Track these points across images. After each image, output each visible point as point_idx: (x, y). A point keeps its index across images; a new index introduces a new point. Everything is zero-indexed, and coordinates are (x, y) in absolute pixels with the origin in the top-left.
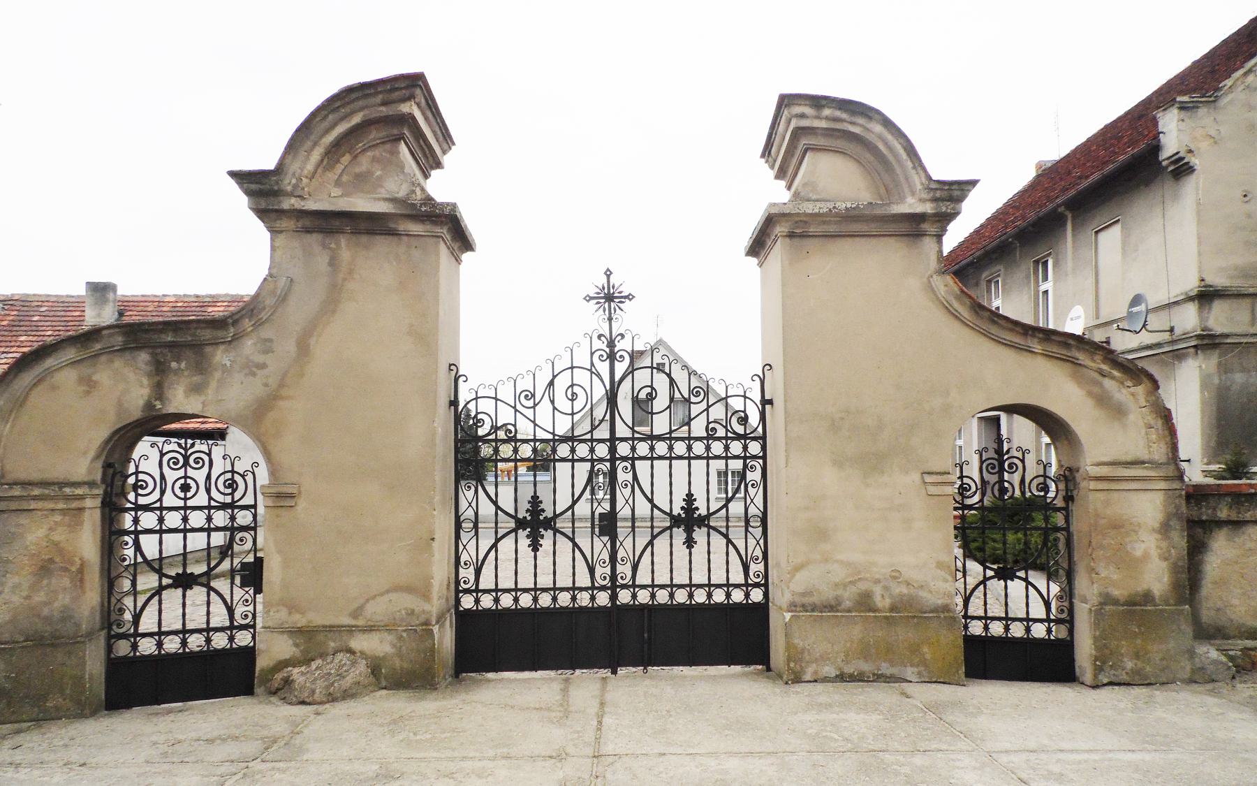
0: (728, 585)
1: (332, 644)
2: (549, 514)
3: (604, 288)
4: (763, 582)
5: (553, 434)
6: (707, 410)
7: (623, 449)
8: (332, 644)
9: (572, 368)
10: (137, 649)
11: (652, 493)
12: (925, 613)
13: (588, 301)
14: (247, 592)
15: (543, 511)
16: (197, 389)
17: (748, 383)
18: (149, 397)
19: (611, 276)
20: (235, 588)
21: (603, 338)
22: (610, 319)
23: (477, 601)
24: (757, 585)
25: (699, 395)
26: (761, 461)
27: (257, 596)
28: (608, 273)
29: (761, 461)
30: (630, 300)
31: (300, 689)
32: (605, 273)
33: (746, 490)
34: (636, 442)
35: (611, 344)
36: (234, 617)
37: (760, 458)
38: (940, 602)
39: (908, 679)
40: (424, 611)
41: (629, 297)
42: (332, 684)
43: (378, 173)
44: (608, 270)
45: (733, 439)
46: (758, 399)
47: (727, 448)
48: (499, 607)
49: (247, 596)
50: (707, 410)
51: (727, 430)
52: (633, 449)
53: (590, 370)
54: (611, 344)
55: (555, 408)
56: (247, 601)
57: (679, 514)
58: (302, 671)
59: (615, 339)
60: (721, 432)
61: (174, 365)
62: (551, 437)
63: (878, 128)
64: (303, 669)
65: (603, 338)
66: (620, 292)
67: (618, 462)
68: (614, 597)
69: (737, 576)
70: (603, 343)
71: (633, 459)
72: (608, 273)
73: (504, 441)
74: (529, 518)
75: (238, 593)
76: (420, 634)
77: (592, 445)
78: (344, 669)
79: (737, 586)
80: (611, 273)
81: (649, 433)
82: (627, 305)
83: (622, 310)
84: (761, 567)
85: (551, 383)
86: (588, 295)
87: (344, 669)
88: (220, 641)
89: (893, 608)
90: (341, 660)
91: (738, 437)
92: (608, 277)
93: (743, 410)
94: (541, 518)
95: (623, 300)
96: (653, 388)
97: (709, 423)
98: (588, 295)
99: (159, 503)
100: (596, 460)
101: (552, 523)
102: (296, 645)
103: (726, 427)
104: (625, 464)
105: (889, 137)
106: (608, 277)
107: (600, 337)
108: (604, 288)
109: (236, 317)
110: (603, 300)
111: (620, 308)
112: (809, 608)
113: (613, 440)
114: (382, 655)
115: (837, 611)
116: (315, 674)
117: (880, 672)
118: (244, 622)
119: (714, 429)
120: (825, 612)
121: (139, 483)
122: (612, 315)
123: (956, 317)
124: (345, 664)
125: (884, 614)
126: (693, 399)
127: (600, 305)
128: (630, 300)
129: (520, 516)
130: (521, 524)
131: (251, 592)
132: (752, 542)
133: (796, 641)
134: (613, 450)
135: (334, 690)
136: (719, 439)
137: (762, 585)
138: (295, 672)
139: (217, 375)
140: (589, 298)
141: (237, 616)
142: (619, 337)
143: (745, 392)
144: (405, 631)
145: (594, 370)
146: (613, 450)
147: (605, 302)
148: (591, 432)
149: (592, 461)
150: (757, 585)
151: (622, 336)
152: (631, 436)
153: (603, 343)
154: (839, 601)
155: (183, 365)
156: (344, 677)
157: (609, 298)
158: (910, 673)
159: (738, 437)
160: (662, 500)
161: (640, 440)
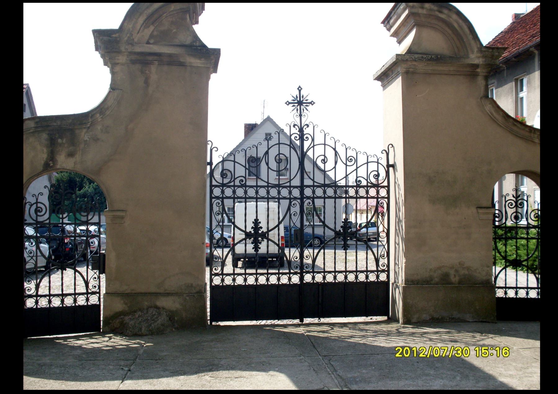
0: (367, 271)
1: (146, 303)
2: (264, 230)
3: (297, 97)
4: (386, 269)
5: (268, 183)
6: (356, 170)
7: (308, 192)
8: (146, 303)
9: (279, 144)
10: (38, 304)
11: (324, 217)
12: (476, 284)
13: (288, 105)
14: (95, 273)
15: (261, 228)
16: (71, 155)
17: (380, 155)
18: (47, 159)
19: (302, 91)
20: (89, 270)
21: (296, 127)
22: (301, 115)
23: (223, 280)
24: (383, 271)
25: (352, 160)
26: (386, 200)
27: (101, 275)
28: (300, 88)
29: (386, 200)
30: (312, 105)
31: (132, 327)
32: (298, 89)
33: (290, 215)
34: (315, 188)
35: (301, 130)
36: (88, 287)
37: (386, 198)
38: (484, 278)
39: (468, 320)
40: (198, 284)
41: (312, 103)
42: (151, 325)
43: (174, 31)
44: (300, 87)
45: (371, 187)
46: (385, 164)
47: (367, 192)
48: (236, 284)
49: (95, 276)
50: (356, 170)
51: (368, 182)
52: (314, 192)
53: (290, 146)
54: (301, 130)
55: (269, 168)
56: (95, 278)
57: (340, 231)
58: (130, 318)
59: (303, 127)
60: (364, 183)
61: (60, 141)
62: (266, 184)
63: (454, 17)
64: (130, 317)
65: (296, 127)
66: (307, 100)
67: (305, 200)
68: (302, 278)
69: (372, 266)
70: (296, 129)
71: (223, 198)
72: (300, 88)
73: (239, 187)
74: (253, 232)
75: (91, 273)
76: (197, 297)
77: (290, 189)
78: (155, 317)
79: (372, 272)
80: (301, 89)
81: (323, 183)
82: (310, 107)
83: (307, 110)
84: (386, 261)
85: (267, 153)
86: (288, 101)
87: (155, 317)
88: (81, 301)
89: (460, 282)
90: (153, 312)
91: (374, 186)
92: (300, 91)
93: (377, 170)
94: (260, 232)
95: (308, 105)
96: (325, 157)
97: (357, 177)
98: (288, 101)
99: (48, 220)
100: (292, 198)
101: (267, 235)
102: (126, 304)
103: (367, 180)
104: (218, 201)
105: (460, 21)
106: (300, 91)
107: (294, 126)
108: (297, 97)
109: (92, 113)
110: (297, 104)
111: (306, 109)
112: (416, 283)
113: (302, 187)
114: (175, 309)
115: (431, 284)
116: (139, 319)
117: (453, 317)
118: (94, 290)
119: (360, 181)
120: (424, 285)
121: (38, 209)
122: (302, 113)
123: (495, 121)
124: (155, 314)
125: (456, 285)
126: (348, 163)
127: (295, 107)
128: (312, 105)
129: (248, 231)
130: (248, 235)
131: (98, 273)
133: (408, 301)
134: (302, 193)
135: (152, 328)
136: (363, 187)
137: (386, 271)
138: (127, 318)
139: (82, 146)
140: (288, 103)
141: (90, 286)
142: (306, 126)
143: (378, 160)
144: (187, 296)
145: (291, 146)
146: (302, 193)
147: (298, 106)
148: (290, 182)
149: (290, 199)
150: (383, 271)
151: (308, 126)
152: (312, 184)
153: (296, 129)
154: (431, 278)
155: (64, 141)
156: (156, 322)
157: (300, 103)
158: (468, 317)
159: (374, 186)
160: (330, 222)
161: (318, 187)
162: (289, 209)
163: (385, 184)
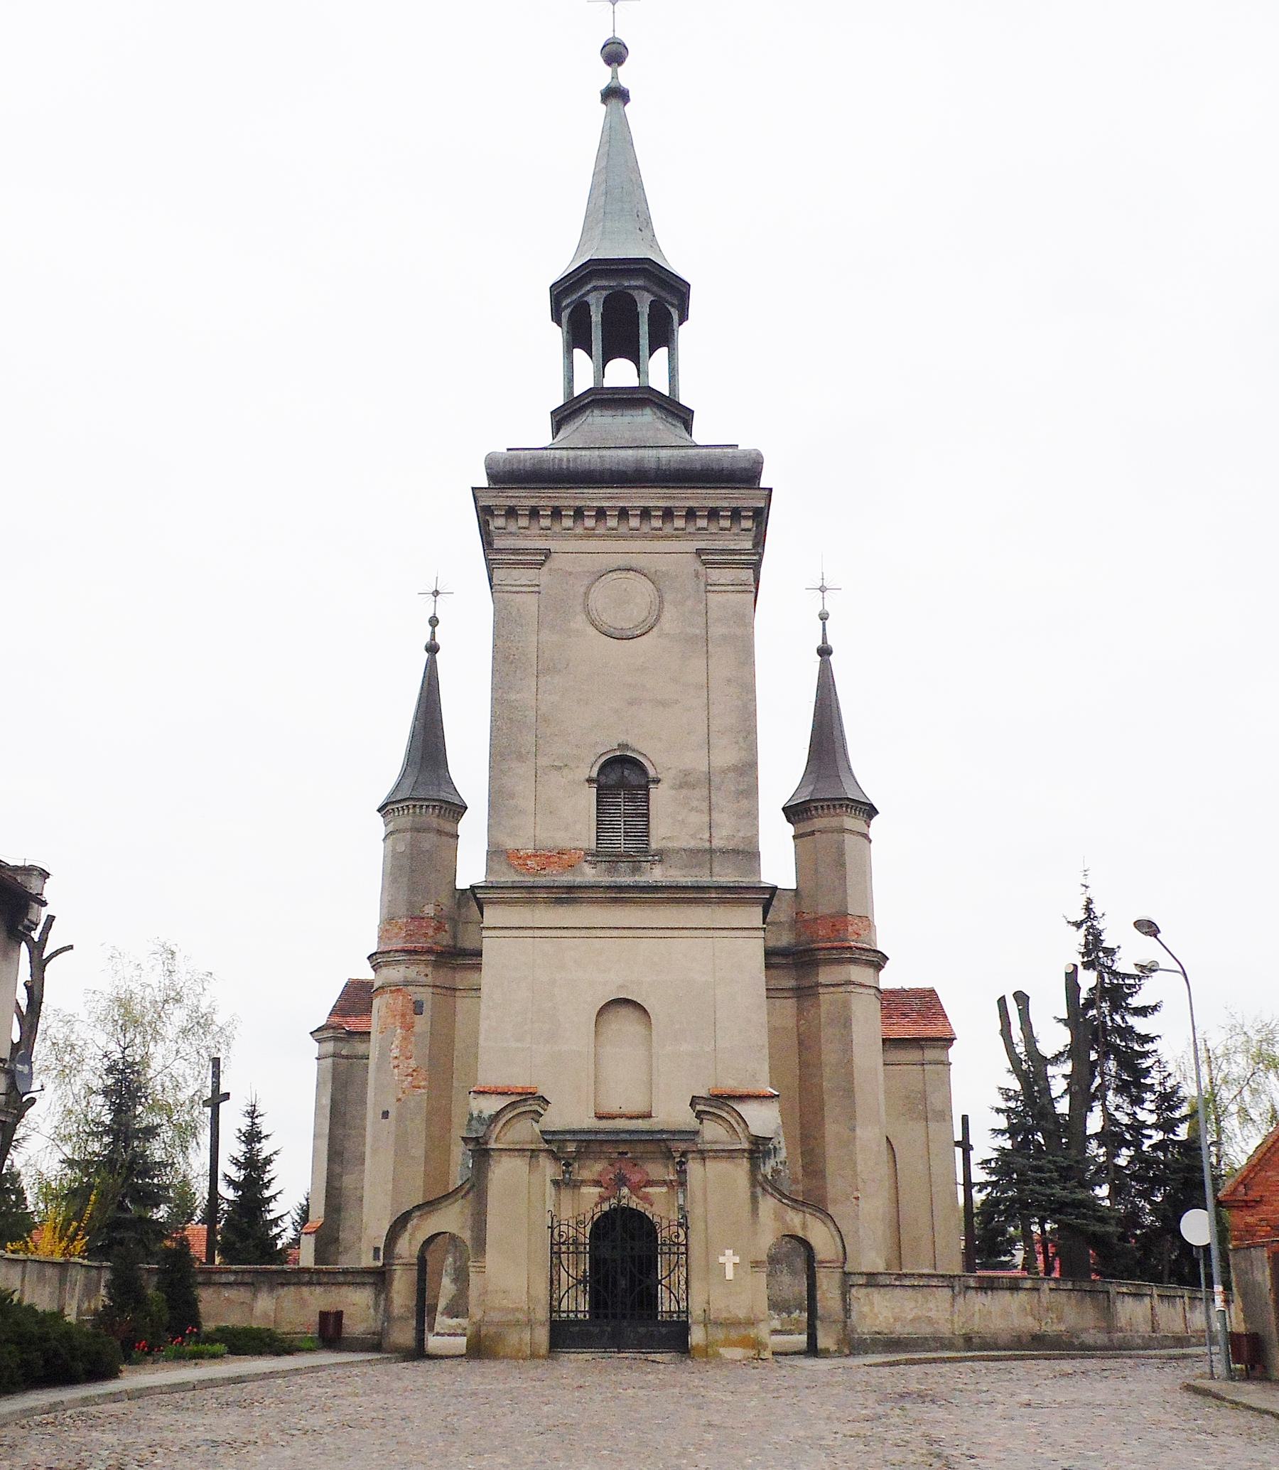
84: (685, 1304)
132: (681, 1292)
162: (560, 1304)
163: (684, 1242)
